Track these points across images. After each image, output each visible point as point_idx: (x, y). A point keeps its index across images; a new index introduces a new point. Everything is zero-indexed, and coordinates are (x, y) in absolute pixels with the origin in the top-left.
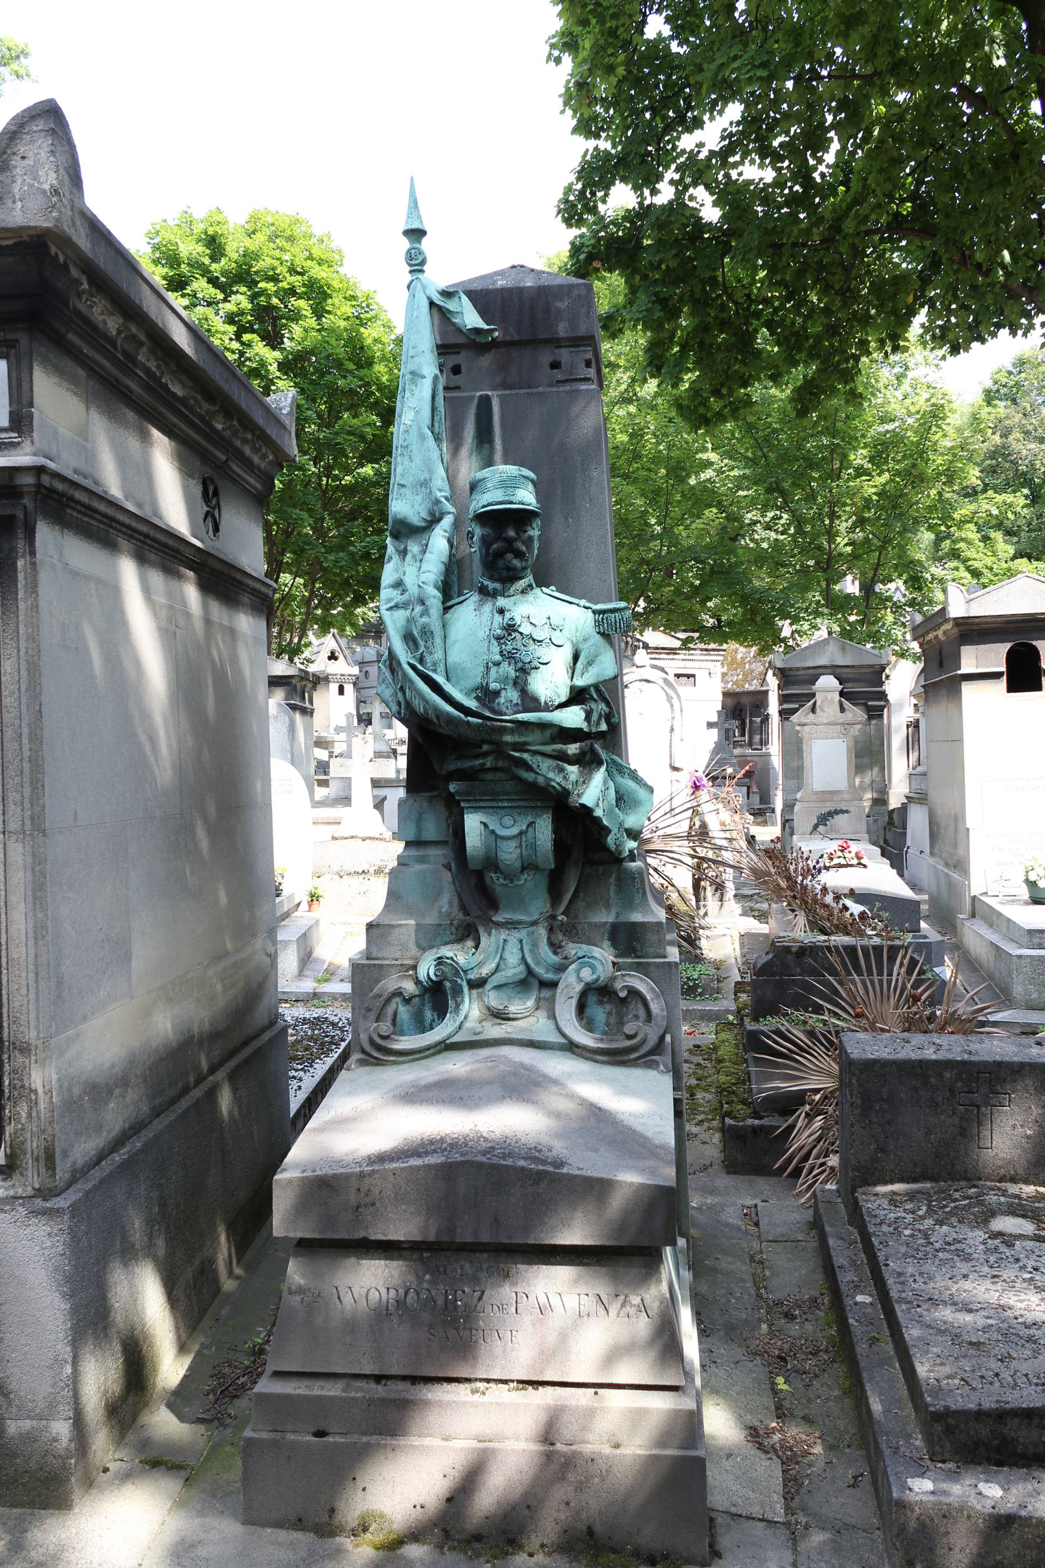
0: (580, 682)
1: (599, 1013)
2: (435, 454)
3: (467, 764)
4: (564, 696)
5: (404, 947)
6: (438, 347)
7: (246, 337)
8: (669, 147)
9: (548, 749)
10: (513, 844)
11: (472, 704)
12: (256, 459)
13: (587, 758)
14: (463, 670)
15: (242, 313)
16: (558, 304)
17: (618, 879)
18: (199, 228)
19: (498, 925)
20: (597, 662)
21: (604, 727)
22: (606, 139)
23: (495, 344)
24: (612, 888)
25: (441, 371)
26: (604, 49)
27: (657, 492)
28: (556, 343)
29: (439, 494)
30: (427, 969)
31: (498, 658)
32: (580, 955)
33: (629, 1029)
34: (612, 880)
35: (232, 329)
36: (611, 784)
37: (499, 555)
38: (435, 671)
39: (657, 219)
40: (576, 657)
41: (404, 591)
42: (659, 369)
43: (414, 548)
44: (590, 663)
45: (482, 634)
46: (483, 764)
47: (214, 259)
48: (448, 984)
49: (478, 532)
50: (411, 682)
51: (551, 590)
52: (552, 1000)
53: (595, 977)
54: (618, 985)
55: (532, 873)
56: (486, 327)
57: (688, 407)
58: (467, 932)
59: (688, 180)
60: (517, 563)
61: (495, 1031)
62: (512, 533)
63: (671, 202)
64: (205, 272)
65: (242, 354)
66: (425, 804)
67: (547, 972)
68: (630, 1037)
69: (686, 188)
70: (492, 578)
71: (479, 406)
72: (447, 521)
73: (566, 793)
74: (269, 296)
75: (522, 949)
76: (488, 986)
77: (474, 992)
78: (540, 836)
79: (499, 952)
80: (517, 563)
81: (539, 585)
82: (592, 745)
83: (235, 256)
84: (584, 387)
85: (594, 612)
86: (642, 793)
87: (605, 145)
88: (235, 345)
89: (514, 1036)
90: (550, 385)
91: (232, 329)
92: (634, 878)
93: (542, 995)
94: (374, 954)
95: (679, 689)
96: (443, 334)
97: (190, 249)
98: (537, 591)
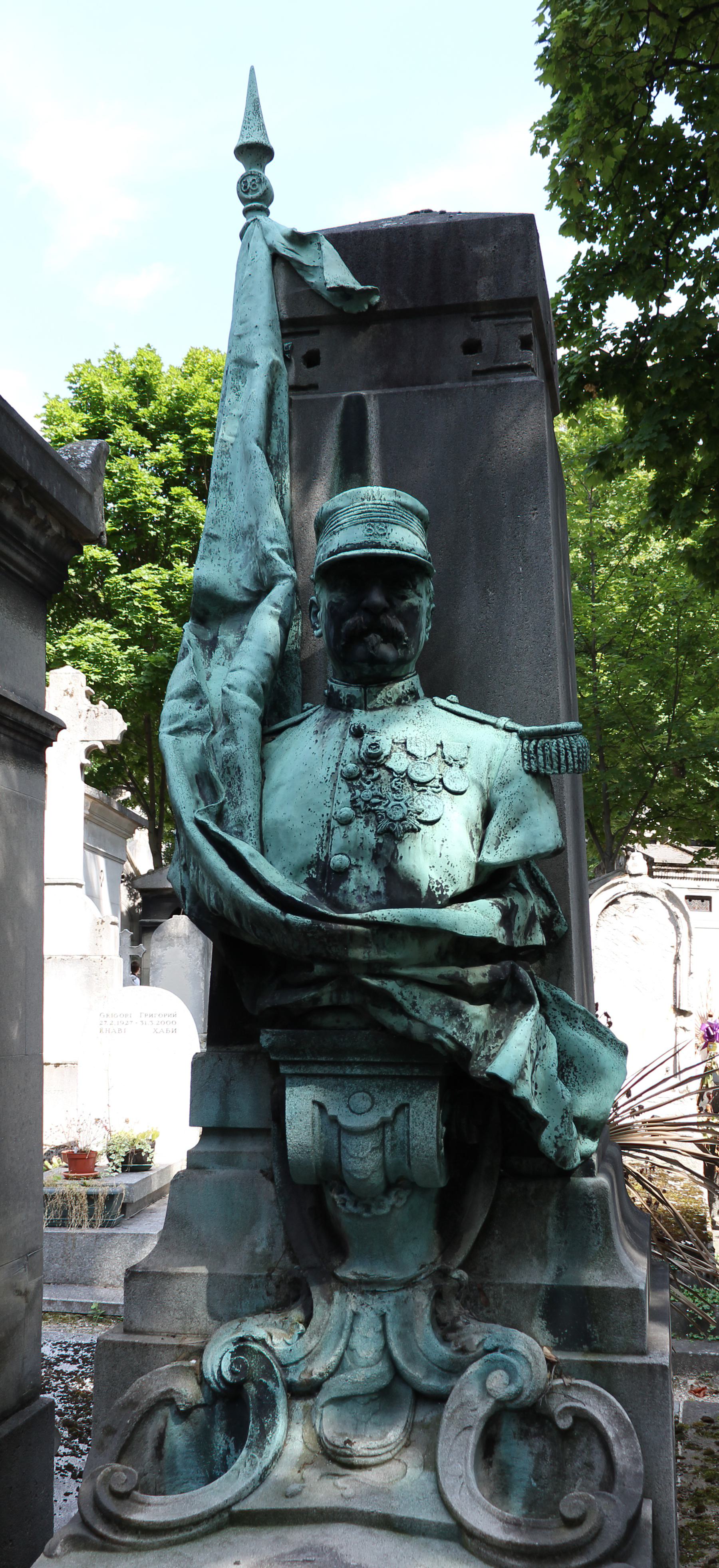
0: (492, 857)
1: (521, 1455)
2: (266, 482)
3: (290, 998)
4: (464, 880)
5: (188, 1314)
6: (283, 323)
7: (175, 490)
8: (681, 251)
9: (432, 974)
10: (369, 1143)
11: (297, 891)
12: (28, 528)
13: (506, 991)
14: (288, 833)
15: (171, 463)
16: (479, 250)
17: (562, 1207)
18: (126, 369)
19: (346, 1285)
20: (524, 821)
21: (539, 938)
22: (603, 242)
23: (373, 316)
24: (551, 1222)
25: (287, 360)
26: (598, 120)
27: (665, 673)
28: (473, 311)
29: (268, 546)
30: (218, 1360)
31: (347, 811)
32: (488, 1345)
33: (570, 1506)
34: (552, 1208)
35: (159, 481)
36: (551, 1039)
37: (357, 636)
38: (240, 835)
39: (665, 331)
40: (487, 814)
41: (202, 703)
42: (666, 514)
43: (228, 637)
44: (513, 823)
45: (322, 773)
46: (316, 999)
47: (143, 402)
48: (252, 1389)
49: (323, 598)
50: (197, 853)
51: (451, 701)
52: (433, 1429)
53: (513, 1389)
54: (558, 1405)
55: (404, 1195)
56: (359, 287)
57: (704, 561)
58: (290, 1294)
59: (704, 286)
60: (387, 651)
61: (324, 1491)
62: (377, 598)
63: (681, 314)
64: (131, 416)
65: (169, 510)
66: (236, 1065)
67: (429, 1373)
68: (571, 1524)
69: (701, 297)
70: (347, 680)
71: (345, 415)
72: (280, 591)
73: (463, 1054)
74: (203, 444)
75: (384, 1332)
76: (322, 1398)
77: (299, 1405)
78: (417, 1130)
79: (337, 1338)
80: (387, 651)
81: (430, 694)
82: (513, 970)
83: (166, 399)
84: (517, 379)
85: (522, 736)
86: (606, 1055)
87: (598, 247)
88: (162, 501)
89: (357, 1505)
90: (463, 378)
91: (159, 481)
92: (589, 1206)
93: (419, 1418)
94: (138, 1324)
95: (691, 914)
96: (292, 300)
97: (114, 391)
98: (427, 703)
